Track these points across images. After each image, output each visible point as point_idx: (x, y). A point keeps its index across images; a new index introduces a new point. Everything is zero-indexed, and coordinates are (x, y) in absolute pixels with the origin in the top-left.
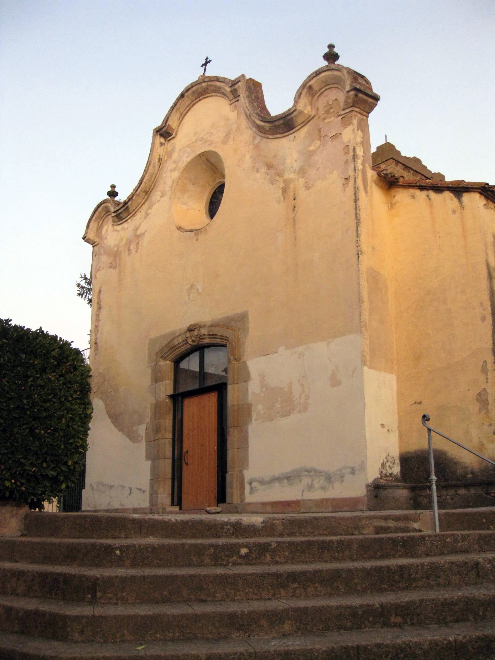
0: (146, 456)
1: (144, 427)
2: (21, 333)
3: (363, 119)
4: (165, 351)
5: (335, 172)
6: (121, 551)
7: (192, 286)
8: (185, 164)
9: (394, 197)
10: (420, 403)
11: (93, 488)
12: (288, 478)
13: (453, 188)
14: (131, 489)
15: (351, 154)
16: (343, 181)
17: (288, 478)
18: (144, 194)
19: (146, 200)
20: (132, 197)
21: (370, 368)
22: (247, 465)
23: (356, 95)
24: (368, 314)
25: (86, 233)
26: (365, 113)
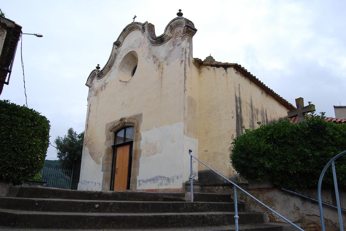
0: (102, 170)
1: (102, 158)
2: (14, 107)
3: (190, 38)
4: (112, 128)
5: (178, 59)
6: (38, 204)
7: (123, 103)
8: (124, 56)
9: (201, 69)
10: (207, 151)
11: (82, 183)
12: (153, 180)
13: (224, 65)
14: (95, 183)
15: (184, 51)
16: (181, 62)
17: (153, 180)
18: (108, 67)
19: (109, 70)
20: (104, 69)
21: (187, 136)
22: (138, 174)
23: (187, 28)
24: (187, 114)
25: (87, 82)
26: (191, 36)
